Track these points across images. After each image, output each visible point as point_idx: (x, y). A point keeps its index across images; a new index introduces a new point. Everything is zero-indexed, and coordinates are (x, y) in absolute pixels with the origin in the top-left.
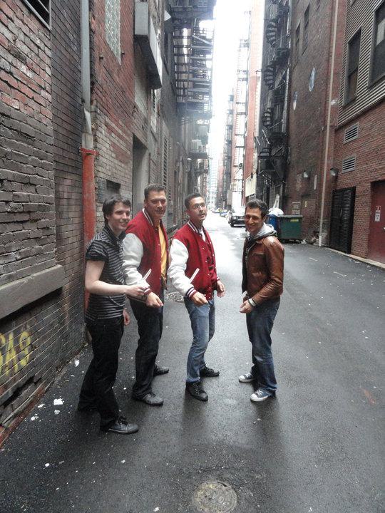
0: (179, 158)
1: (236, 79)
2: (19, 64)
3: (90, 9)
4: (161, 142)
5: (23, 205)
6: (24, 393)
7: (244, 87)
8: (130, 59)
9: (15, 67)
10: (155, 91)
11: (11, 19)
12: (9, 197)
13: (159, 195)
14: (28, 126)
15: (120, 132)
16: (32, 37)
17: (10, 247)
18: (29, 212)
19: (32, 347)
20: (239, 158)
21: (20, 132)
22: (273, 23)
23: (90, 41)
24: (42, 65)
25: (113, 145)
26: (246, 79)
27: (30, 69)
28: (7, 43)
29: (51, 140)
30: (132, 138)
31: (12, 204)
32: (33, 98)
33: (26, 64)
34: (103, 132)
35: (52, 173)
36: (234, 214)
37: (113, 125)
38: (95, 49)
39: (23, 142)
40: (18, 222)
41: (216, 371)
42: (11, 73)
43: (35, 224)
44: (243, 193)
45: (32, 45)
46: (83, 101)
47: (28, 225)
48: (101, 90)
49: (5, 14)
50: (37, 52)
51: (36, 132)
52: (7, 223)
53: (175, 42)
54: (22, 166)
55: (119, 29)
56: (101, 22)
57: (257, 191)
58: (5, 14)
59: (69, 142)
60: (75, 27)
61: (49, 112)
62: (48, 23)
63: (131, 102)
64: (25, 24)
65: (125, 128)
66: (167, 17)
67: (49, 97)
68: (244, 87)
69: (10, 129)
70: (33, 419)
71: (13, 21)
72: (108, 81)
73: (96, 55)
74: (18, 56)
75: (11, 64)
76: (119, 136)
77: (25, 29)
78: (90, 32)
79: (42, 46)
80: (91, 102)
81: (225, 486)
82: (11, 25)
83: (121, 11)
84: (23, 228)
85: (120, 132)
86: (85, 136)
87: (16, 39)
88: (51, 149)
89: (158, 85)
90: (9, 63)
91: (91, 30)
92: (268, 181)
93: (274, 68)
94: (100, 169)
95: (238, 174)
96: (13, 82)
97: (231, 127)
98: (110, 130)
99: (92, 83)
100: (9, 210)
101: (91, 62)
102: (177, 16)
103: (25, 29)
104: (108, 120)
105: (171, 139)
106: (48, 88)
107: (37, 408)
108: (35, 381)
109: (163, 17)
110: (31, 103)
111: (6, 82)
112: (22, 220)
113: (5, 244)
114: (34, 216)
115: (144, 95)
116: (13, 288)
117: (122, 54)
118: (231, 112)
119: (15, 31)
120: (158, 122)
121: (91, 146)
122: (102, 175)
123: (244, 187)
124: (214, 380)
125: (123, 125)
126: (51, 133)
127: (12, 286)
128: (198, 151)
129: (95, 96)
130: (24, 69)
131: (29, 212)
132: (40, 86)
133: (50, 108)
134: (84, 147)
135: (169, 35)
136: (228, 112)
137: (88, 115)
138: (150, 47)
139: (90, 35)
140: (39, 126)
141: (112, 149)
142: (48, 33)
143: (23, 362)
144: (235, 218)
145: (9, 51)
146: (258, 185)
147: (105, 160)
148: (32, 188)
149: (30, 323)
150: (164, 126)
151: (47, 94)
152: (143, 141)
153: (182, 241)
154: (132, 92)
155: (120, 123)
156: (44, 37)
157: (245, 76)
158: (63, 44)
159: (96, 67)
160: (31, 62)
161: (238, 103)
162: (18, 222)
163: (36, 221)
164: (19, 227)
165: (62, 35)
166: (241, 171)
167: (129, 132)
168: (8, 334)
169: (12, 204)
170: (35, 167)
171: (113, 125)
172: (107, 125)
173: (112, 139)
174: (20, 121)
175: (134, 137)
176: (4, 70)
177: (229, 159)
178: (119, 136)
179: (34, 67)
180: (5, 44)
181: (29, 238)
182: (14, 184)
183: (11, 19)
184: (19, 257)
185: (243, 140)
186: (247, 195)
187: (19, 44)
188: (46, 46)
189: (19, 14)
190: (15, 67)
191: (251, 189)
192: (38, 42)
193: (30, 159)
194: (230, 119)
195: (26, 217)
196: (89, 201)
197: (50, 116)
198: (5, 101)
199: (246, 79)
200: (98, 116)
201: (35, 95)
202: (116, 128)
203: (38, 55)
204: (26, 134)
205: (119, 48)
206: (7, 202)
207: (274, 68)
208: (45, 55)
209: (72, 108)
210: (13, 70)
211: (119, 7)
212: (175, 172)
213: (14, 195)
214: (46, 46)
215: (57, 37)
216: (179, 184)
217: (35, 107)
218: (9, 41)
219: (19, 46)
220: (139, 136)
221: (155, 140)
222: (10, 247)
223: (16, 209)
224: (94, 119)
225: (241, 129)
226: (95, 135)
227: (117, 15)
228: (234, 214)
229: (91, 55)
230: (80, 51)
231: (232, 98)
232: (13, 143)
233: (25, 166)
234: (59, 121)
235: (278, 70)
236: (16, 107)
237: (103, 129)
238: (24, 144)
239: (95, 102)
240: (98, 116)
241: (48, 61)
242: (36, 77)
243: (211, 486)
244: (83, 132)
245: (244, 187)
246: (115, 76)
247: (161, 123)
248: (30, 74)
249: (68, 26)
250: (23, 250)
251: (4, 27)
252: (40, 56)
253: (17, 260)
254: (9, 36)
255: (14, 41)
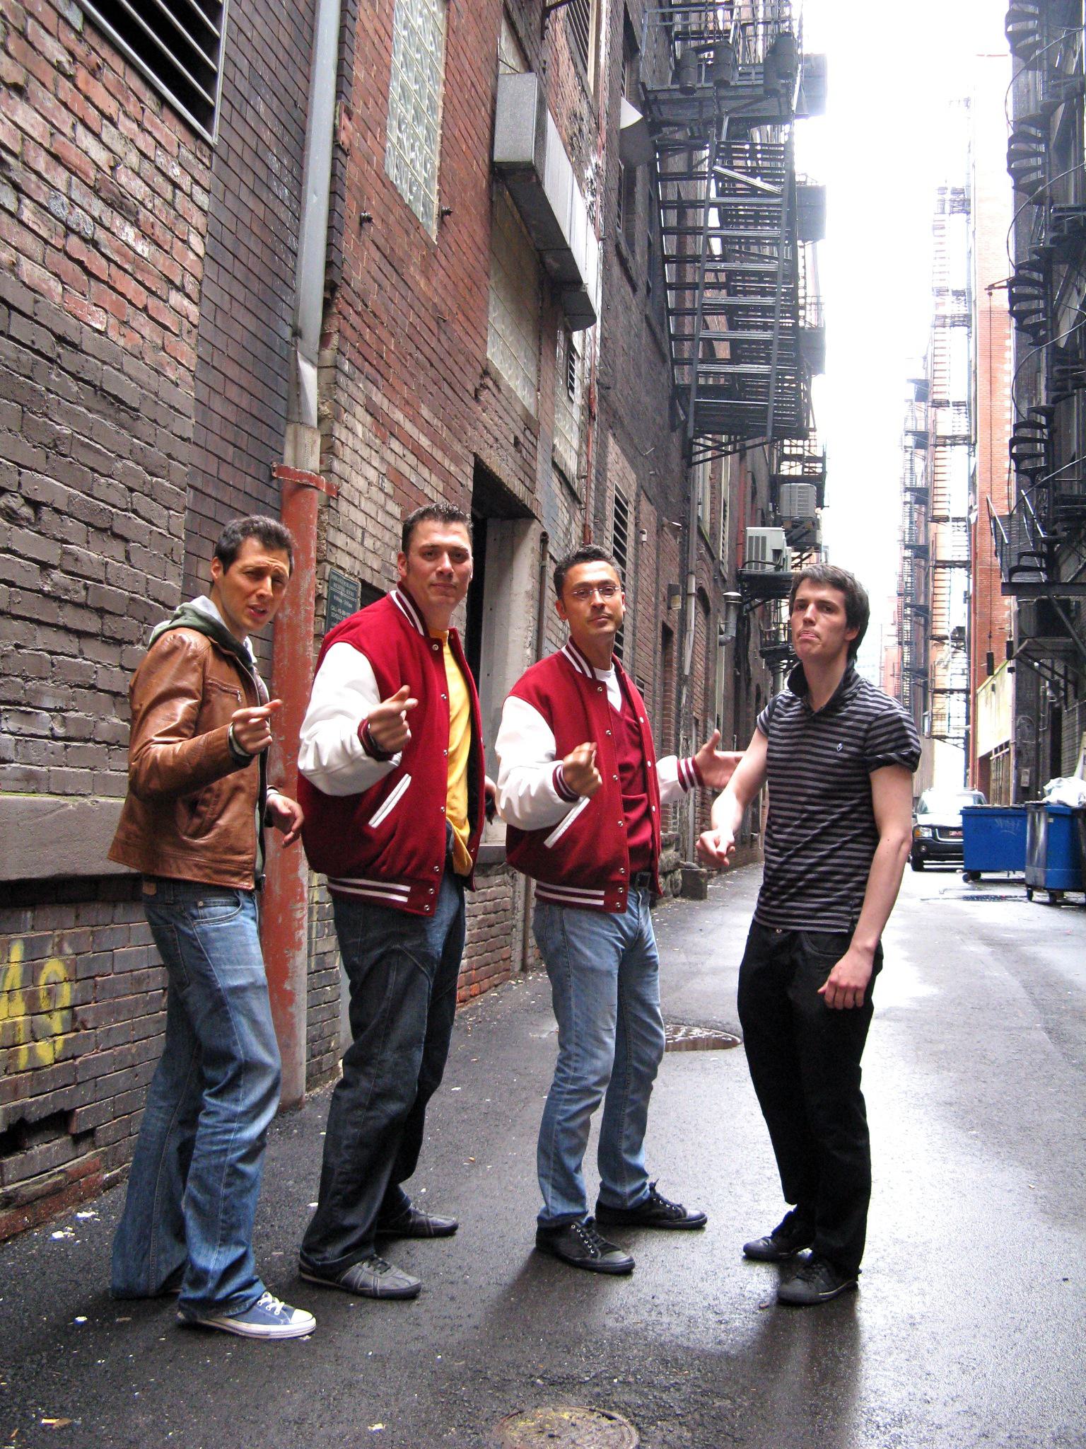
0: (685, 583)
1: (931, 320)
2: (118, 221)
3: (339, 93)
4: (600, 511)
5: (86, 588)
6: (38, 1149)
7: (958, 345)
8: (471, 228)
9: (108, 229)
10: (577, 337)
11: (110, 120)
12: (51, 553)
13: (445, 533)
14: (123, 377)
15: (424, 442)
16: (161, 160)
17: (38, 692)
18: (101, 612)
19: (75, 1023)
20: (952, 611)
21: (99, 390)
22: (1033, 131)
23: (333, 175)
24: (181, 227)
25: (396, 477)
26: (966, 321)
27: (145, 235)
28: (92, 173)
29: (187, 427)
30: (470, 471)
31: (57, 575)
32: (145, 309)
33: (136, 224)
34: (359, 429)
35: (179, 521)
36: (922, 819)
37: (398, 416)
38: (347, 195)
39: (105, 416)
40: (67, 630)
41: (692, 1212)
42: (95, 244)
43: (115, 650)
44: (969, 741)
45: (159, 179)
46: (297, 333)
47: (93, 649)
48: (360, 308)
49: (97, 108)
50: (169, 196)
51: (145, 397)
52: (39, 623)
53: (670, 192)
54: (94, 480)
55: (437, 148)
56: (376, 127)
57: (1018, 729)
58: (97, 108)
59: (244, 441)
60: (287, 139)
61: (187, 352)
62: (210, 132)
63: (470, 358)
64: (144, 130)
65: (445, 433)
66: (630, 116)
67: (193, 311)
68: (958, 345)
69: (77, 378)
70: (58, 1235)
71: (114, 124)
72: (386, 283)
73: (351, 210)
74: (119, 204)
75: (98, 221)
76: (417, 451)
77: (144, 142)
78: (334, 151)
79: (185, 182)
80: (324, 339)
81: (611, 1418)
82: (108, 133)
83: (447, 100)
84: (81, 652)
85: (424, 442)
86: (296, 436)
87: (117, 165)
88: (183, 451)
89: (585, 317)
90: (93, 218)
91: (337, 145)
92: (1054, 686)
93: (1048, 273)
94: (340, 540)
95: (951, 668)
96: (98, 265)
97: (921, 497)
98: (384, 427)
99: (331, 288)
100: (47, 588)
101: (330, 227)
102: (667, 113)
103: (144, 142)
104: (378, 398)
105: (646, 507)
106: (191, 287)
107: (74, 1216)
108: (76, 1128)
109: (614, 114)
110: (140, 321)
111: (80, 263)
112: (80, 627)
113: (26, 679)
114: (112, 626)
115: (530, 353)
116: (36, 811)
117: (443, 214)
118: (922, 440)
119: (118, 147)
120: (585, 438)
121: (312, 462)
122: (346, 562)
123: (971, 718)
124: (681, 1242)
125: (435, 422)
126: (188, 406)
127: (31, 802)
128: (770, 569)
129: (335, 323)
130: (129, 233)
131: (101, 612)
132: (171, 282)
133: (192, 341)
134: (288, 461)
135: (641, 174)
136: (910, 441)
137: (309, 374)
138: (543, 193)
139: (334, 159)
140: (154, 382)
141: (388, 487)
142: (207, 152)
143: (45, 1052)
144: (927, 834)
145: (96, 191)
146: (1022, 705)
147: (360, 518)
148: (117, 548)
149: (74, 940)
150: (611, 458)
151: (186, 302)
152: (518, 489)
153: (529, 699)
154: (478, 330)
155: (425, 412)
156: (194, 161)
157: (963, 310)
158: (249, 178)
159: (348, 244)
160: (152, 218)
161: (938, 404)
162: (67, 630)
163: (119, 642)
164: (72, 645)
165: (248, 157)
166: (962, 655)
167: (458, 448)
168: (10, 942)
169: (57, 575)
170: (131, 490)
171: (398, 416)
172: (371, 410)
173: (391, 458)
174: (104, 363)
175: (482, 474)
176: (78, 234)
177: (919, 611)
178: (417, 451)
179: (159, 231)
180: (87, 176)
181: (92, 687)
182: (70, 523)
183: (110, 120)
184: (60, 731)
185: (963, 538)
186: (981, 752)
187: (124, 177)
188: (197, 183)
189: (132, 107)
190: (108, 229)
191: (997, 723)
192: (175, 172)
193: (119, 465)
194: (919, 466)
195: (91, 623)
196: (293, 628)
197: (190, 359)
198: (71, 306)
199: (966, 321)
200: (342, 379)
201: (152, 303)
202: (408, 426)
203: (171, 205)
204: (115, 397)
205: (435, 198)
206: (45, 566)
207: (1048, 273)
208: (191, 205)
209: (259, 349)
210: (101, 235)
211: (441, 89)
212: (667, 633)
213: (65, 552)
214: (197, 183)
215: (233, 161)
216: (683, 680)
217: (158, 338)
218: (99, 168)
219: (123, 179)
220: (504, 468)
221: (573, 496)
222: (38, 692)
223: (67, 591)
224: (329, 389)
225: (955, 498)
226: (328, 437)
227: (432, 108)
228: (922, 819)
229: (332, 210)
230: (299, 198)
231: (923, 392)
232: (79, 414)
233: (103, 480)
234: (215, 379)
235: (1067, 279)
236: (98, 326)
237: (360, 423)
238: (108, 423)
239: (335, 340)
240: (342, 379)
241: (198, 219)
242: (161, 258)
243: (566, 1416)
244: (289, 421)
245: (971, 718)
246: (413, 272)
247: (603, 446)
248: (143, 248)
249: (267, 136)
250: (72, 714)
251: (90, 136)
252: (178, 207)
253: (55, 738)
254: (101, 156)
255: (112, 168)
